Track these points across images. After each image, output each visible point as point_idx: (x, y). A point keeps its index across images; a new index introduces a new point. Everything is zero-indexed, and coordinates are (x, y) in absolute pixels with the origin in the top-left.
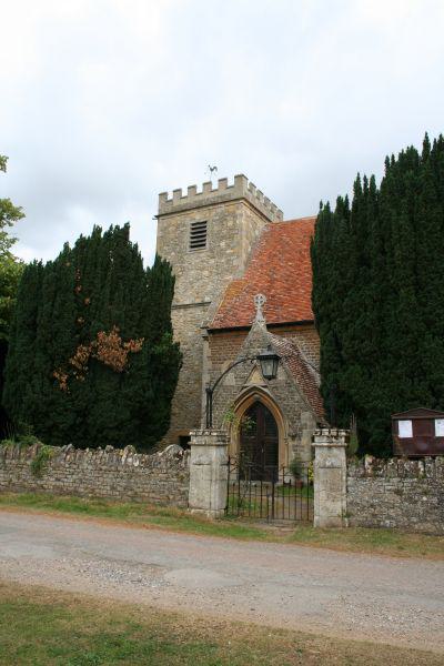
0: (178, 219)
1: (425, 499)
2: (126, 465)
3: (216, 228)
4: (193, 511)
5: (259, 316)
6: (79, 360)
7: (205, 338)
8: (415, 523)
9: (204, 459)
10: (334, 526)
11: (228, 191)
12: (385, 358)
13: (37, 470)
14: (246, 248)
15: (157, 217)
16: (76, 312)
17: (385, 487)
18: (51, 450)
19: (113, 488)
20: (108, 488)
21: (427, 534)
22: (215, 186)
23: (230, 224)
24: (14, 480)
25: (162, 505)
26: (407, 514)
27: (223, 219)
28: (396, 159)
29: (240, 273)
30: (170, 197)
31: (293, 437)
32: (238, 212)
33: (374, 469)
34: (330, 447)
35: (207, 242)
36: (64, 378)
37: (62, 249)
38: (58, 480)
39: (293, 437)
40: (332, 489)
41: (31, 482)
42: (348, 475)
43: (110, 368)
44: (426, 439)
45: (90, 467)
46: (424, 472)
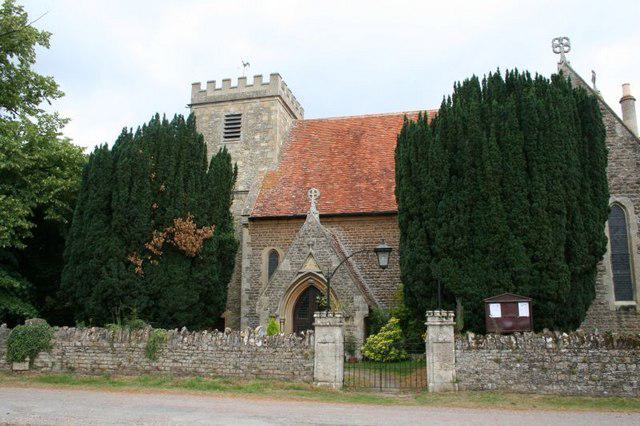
0: (212, 109)
1: (518, 365)
2: (249, 345)
3: (251, 122)
4: (319, 384)
5: (313, 209)
6: (155, 246)
7: (246, 225)
8: (511, 385)
9: (328, 338)
10: (446, 391)
11: (263, 88)
12: (473, 252)
13: (151, 352)
14: (279, 142)
15: (190, 106)
16: (152, 199)
17: (486, 358)
18: (161, 332)
19: (236, 367)
20: (231, 367)
21: (522, 393)
22: (250, 81)
23: (265, 118)
24: (125, 363)
25: (288, 380)
26: (505, 378)
27: (257, 114)
28: (462, 85)
29: (274, 166)
30: (204, 87)
31: (347, 318)
32: (273, 108)
33: (477, 343)
34: (441, 326)
35: (241, 134)
36: (140, 263)
37: (119, 133)
38: (175, 361)
39: (347, 318)
40: (445, 359)
41: (144, 363)
42: (456, 349)
43: (183, 253)
44: (512, 319)
45: (210, 348)
46: (517, 344)
